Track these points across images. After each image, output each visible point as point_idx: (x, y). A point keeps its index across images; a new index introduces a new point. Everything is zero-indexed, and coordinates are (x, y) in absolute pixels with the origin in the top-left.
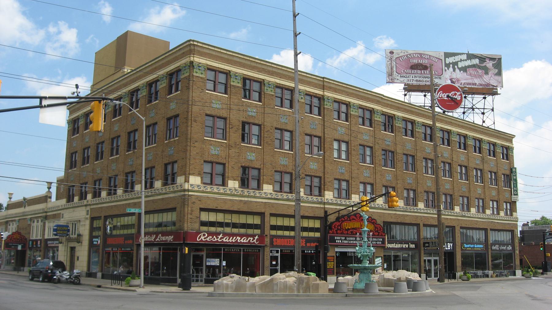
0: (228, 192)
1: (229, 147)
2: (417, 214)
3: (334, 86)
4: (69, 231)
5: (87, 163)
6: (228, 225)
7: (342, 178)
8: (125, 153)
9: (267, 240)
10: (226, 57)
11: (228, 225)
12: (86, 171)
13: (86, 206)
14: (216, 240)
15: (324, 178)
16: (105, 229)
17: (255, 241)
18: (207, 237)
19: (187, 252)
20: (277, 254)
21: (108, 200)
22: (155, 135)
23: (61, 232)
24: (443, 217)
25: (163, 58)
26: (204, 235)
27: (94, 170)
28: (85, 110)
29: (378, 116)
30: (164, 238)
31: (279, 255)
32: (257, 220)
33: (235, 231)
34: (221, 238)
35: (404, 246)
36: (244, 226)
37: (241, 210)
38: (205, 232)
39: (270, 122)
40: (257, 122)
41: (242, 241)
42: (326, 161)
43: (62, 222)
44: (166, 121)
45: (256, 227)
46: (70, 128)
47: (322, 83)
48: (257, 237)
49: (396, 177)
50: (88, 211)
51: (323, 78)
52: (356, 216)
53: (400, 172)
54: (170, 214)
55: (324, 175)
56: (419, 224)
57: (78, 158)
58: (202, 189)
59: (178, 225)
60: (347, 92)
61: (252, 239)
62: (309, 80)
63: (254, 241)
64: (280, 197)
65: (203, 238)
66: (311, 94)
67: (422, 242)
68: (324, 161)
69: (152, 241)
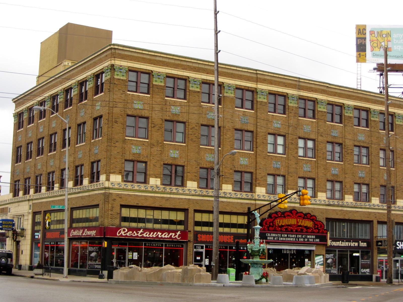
0: (150, 189)
1: (152, 145)
2: (370, 210)
3: (269, 78)
4: (14, 225)
5: (30, 158)
6: (149, 221)
7: (277, 173)
8: (60, 150)
9: (191, 236)
10: (148, 57)
11: (149, 221)
12: (38, 164)
13: (29, 200)
14: (136, 235)
15: (256, 173)
16: (45, 224)
17: (177, 236)
18: (127, 232)
19: (106, 246)
20: (201, 250)
21: (46, 196)
22: (85, 133)
23: (7, 226)
24: (393, 212)
25: (90, 60)
26: (124, 230)
27: (35, 166)
28: (28, 105)
29: (323, 107)
30: (89, 233)
31: (203, 251)
32: (180, 216)
33: (157, 226)
34: (141, 234)
35: (352, 244)
36: (165, 222)
37: (163, 207)
38: (125, 227)
39: (194, 120)
40: (181, 119)
41: (163, 236)
42: (258, 156)
43: (9, 217)
44: (92, 121)
45: (180, 223)
46: (16, 122)
47: (255, 76)
48: (179, 233)
49: (344, 171)
50: (30, 206)
51: (256, 70)
52: (292, 213)
53: (349, 166)
54: (95, 210)
55: (256, 170)
56: (372, 221)
57: (23, 153)
58: (123, 186)
59: (100, 220)
60: (284, 83)
61: (174, 234)
62: (240, 73)
63: (176, 236)
64: (205, 193)
65: (123, 233)
66: (243, 87)
67: (375, 240)
68: (256, 156)
69: (80, 236)
